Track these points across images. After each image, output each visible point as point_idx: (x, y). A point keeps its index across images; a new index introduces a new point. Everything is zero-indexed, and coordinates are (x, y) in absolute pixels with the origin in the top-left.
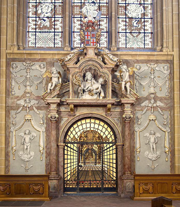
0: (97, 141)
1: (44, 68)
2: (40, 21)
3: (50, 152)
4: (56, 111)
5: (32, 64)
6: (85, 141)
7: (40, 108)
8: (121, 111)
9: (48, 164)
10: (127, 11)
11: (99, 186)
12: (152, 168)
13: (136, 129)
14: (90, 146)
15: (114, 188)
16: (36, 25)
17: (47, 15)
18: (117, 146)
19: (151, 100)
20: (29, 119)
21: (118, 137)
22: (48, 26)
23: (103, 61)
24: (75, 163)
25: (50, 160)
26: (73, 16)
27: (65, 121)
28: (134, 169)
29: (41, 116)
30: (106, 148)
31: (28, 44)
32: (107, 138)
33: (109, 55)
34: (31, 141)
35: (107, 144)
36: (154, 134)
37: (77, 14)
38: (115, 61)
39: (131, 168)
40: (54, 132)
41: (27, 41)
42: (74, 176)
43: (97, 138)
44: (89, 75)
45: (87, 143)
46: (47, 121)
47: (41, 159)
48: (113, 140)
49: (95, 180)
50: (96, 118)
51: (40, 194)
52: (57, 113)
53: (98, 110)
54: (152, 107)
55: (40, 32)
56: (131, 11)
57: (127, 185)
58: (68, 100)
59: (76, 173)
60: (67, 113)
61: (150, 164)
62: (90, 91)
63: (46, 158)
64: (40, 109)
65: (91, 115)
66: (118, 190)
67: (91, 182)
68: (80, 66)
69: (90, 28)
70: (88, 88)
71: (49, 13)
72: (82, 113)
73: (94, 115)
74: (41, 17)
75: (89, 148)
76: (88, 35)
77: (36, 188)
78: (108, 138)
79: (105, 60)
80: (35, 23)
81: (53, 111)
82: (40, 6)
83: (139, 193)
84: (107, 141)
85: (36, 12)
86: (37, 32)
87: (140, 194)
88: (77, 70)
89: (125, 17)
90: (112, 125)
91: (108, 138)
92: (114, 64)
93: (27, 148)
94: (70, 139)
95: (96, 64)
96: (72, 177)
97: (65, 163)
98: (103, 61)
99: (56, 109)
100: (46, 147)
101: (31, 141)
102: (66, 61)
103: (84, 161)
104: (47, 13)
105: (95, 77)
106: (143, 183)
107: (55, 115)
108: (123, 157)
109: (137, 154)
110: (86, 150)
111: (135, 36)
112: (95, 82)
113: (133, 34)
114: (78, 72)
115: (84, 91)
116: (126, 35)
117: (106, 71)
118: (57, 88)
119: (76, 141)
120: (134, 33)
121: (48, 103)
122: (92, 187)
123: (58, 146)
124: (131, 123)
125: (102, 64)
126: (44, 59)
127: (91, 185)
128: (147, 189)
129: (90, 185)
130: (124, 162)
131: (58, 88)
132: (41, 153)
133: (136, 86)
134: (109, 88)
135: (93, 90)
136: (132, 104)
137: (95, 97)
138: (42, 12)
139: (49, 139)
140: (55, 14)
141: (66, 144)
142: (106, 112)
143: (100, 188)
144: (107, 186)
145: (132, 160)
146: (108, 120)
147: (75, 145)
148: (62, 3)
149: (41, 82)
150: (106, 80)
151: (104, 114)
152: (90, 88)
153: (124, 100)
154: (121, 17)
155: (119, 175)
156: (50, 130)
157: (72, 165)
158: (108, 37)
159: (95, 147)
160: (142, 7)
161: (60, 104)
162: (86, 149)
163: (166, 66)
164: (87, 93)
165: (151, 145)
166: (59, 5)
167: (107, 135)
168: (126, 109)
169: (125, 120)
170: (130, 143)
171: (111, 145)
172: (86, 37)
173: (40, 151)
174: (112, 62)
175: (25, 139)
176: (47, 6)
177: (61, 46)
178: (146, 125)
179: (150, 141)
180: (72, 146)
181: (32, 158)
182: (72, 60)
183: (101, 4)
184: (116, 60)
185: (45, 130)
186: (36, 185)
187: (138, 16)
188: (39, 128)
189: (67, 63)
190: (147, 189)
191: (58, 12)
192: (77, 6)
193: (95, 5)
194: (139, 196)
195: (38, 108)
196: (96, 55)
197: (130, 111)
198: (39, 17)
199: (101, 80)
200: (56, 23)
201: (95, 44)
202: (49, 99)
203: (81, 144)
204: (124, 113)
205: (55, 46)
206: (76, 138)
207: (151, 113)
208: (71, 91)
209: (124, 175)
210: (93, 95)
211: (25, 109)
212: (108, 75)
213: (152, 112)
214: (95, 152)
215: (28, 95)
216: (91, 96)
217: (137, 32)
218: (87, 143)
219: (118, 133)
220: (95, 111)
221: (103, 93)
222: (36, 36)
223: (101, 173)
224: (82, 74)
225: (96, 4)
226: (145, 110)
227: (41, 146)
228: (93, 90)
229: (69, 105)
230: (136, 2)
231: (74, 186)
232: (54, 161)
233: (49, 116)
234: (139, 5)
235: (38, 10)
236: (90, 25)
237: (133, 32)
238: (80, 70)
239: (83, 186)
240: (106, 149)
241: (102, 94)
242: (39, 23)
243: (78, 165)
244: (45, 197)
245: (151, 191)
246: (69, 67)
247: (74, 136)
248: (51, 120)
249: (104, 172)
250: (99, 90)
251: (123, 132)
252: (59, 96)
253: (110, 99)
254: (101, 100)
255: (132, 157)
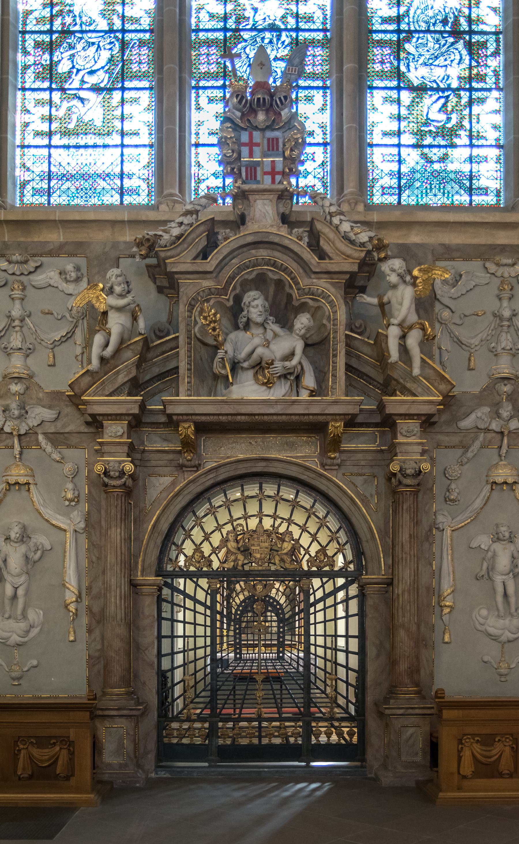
0: (287, 566)
1: (78, 280)
2: (66, 105)
3: (103, 610)
4: (126, 449)
5: (32, 265)
6: (240, 568)
7: (66, 438)
8: (382, 451)
9: (98, 658)
10: (402, 63)
11: (292, 740)
12: (503, 671)
13: (440, 518)
14: (259, 587)
15: (349, 744)
16: (50, 119)
17: (92, 80)
18: (361, 588)
19: (498, 404)
20: (22, 480)
21: (368, 553)
22: (98, 123)
23: (315, 245)
24: (200, 653)
25: (103, 639)
26: (193, 83)
27: (162, 487)
28: (432, 675)
29: (68, 468)
30: (319, 594)
31: (22, 196)
32: (326, 555)
33: (336, 220)
34: (30, 567)
35: (325, 580)
36: (511, 540)
37: (208, 76)
38: (363, 245)
39: (418, 671)
40: (119, 530)
41: (18, 183)
42: (197, 700)
43: (285, 557)
44: (255, 304)
45: (247, 575)
46: (93, 491)
47: (72, 638)
48: (347, 563)
49: (272, 696)
50: (280, 478)
51: (56, 777)
52: (128, 456)
53: (292, 446)
54: (502, 433)
55: (68, 147)
56: (421, 61)
57: (404, 737)
58: (171, 402)
59: (204, 690)
60: (171, 456)
61: (491, 652)
62: (260, 366)
63: (90, 631)
64: (64, 444)
65: (264, 464)
66: (369, 755)
67: (265, 724)
68: (221, 265)
69: (261, 116)
70: (253, 352)
71: (101, 73)
72: (228, 457)
73: (276, 464)
74: (70, 87)
75: (253, 596)
76: (251, 144)
77: (42, 755)
78: (330, 553)
79: (322, 242)
80: (45, 110)
81: (113, 449)
82: (65, 45)
83: (459, 773)
84: (327, 568)
85: (51, 70)
86: (56, 147)
87: (465, 777)
88: (206, 283)
89: (394, 83)
90: (345, 505)
91: (329, 557)
92: (356, 255)
93: (15, 597)
94: (182, 558)
95: (285, 257)
96: (192, 706)
97: (163, 653)
98: (315, 245)
99: (124, 440)
100: (89, 589)
101: (30, 567)
102: (166, 246)
103: (235, 638)
104: (92, 72)
105: (283, 312)
106: (474, 735)
107: (120, 462)
108: (390, 628)
109: (444, 618)
110: (244, 601)
111: (435, 158)
112: (276, 328)
113: (426, 150)
114: (211, 293)
115: (235, 366)
116: (399, 154)
117: (325, 285)
118: (128, 354)
119: (205, 569)
120: (430, 146)
121: (93, 416)
122: (265, 741)
123: (133, 585)
124: (420, 495)
125: (312, 259)
126: (80, 244)
127: (263, 734)
128: (490, 760)
129: (260, 737)
130: (393, 647)
131: (130, 357)
132: (71, 614)
133: (440, 348)
134: (335, 356)
135: (273, 361)
136: (428, 422)
137: (280, 391)
138: (73, 67)
139: (99, 558)
140: (122, 75)
141: (169, 581)
142: (324, 452)
143: (296, 746)
144: (323, 739)
145: (423, 642)
146: (331, 486)
147: (203, 582)
148: (151, 31)
149: (69, 335)
150: (325, 322)
151: (314, 464)
152: (260, 351)
153: (396, 403)
154: (380, 86)
155: (370, 699)
156: (103, 523)
157: (192, 658)
158: (328, 164)
159: (278, 591)
160: (460, 45)
161: (136, 423)
162: (242, 597)
163: (62, 750)
164: (250, 374)
165: (498, 579)
166: (140, 40)
167: (324, 544)
168: (401, 439)
169: (400, 483)
170: (416, 573)
171: (341, 581)
172: (245, 151)
173: (66, 606)
174: (348, 250)
175: (8, 559)
176: (93, 44)
177: (146, 200)
178: (478, 503)
179: (493, 568)
180: (190, 589)
181: (34, 632)
182: (189, 239)
183: (302, 36)
184: (366, 239)
185: (82, 525)
186: (43, 742)
187: (448, 82)
188: (58, 517)
189: (169, 254)
190: (490, 760)
191: (135, 67)
192: (209, 43)
193: (278, 39)
194: (460, 789)
195: (58, 439)
196: (283, 222)
197: (419, 449)
198: (63, 90)
199: (303, 321)
200: (127, 109)
201: (278, 178)
202: (99, 401)
203: (229, 576)
204: (396, 455)
205: (125, 202)
206: (206, 554)
207: (500, 456)
208: (183, 366)
209: (392, 701)
210: (274, 383)
211: (5, 443)
212: (331, 303)
213: (504, 450)
214: (278, 610)
215: (15, 388)
216: (265, 388)
217: (443, 143)
218: (247, 575)
219: (369, 536)
220: (279, 451)
221: (313, 374)
222: (50, 163)
223: (301, 692)
224: (228, 300)
225: (284, 34)
226: (477, 444)
227: (67, 585)
228: (273, 361)
229: (176, 425)
230: (439, 27)
231: (198, 741)
232: (117, 644)
233: (99, 468)
234: (451, 40)
235: (60, 61)
236: (259, 99)
237: (426, 143)
238: (219, 283)
239: (234, 740)
240: (323, 599)
241: (309, 380)
242: (61, 113)
243: (211, 660)
244: (78, 790)
245: (506, 764)
246: (174, 270)
247: (198, 549)
248: (106, 485)
249: (312, 686)
250: (295, 361)
251: (387, 533)
252: (135, 386)
253: (340, 399)
254: (304, 401)
255: (423, 628)
